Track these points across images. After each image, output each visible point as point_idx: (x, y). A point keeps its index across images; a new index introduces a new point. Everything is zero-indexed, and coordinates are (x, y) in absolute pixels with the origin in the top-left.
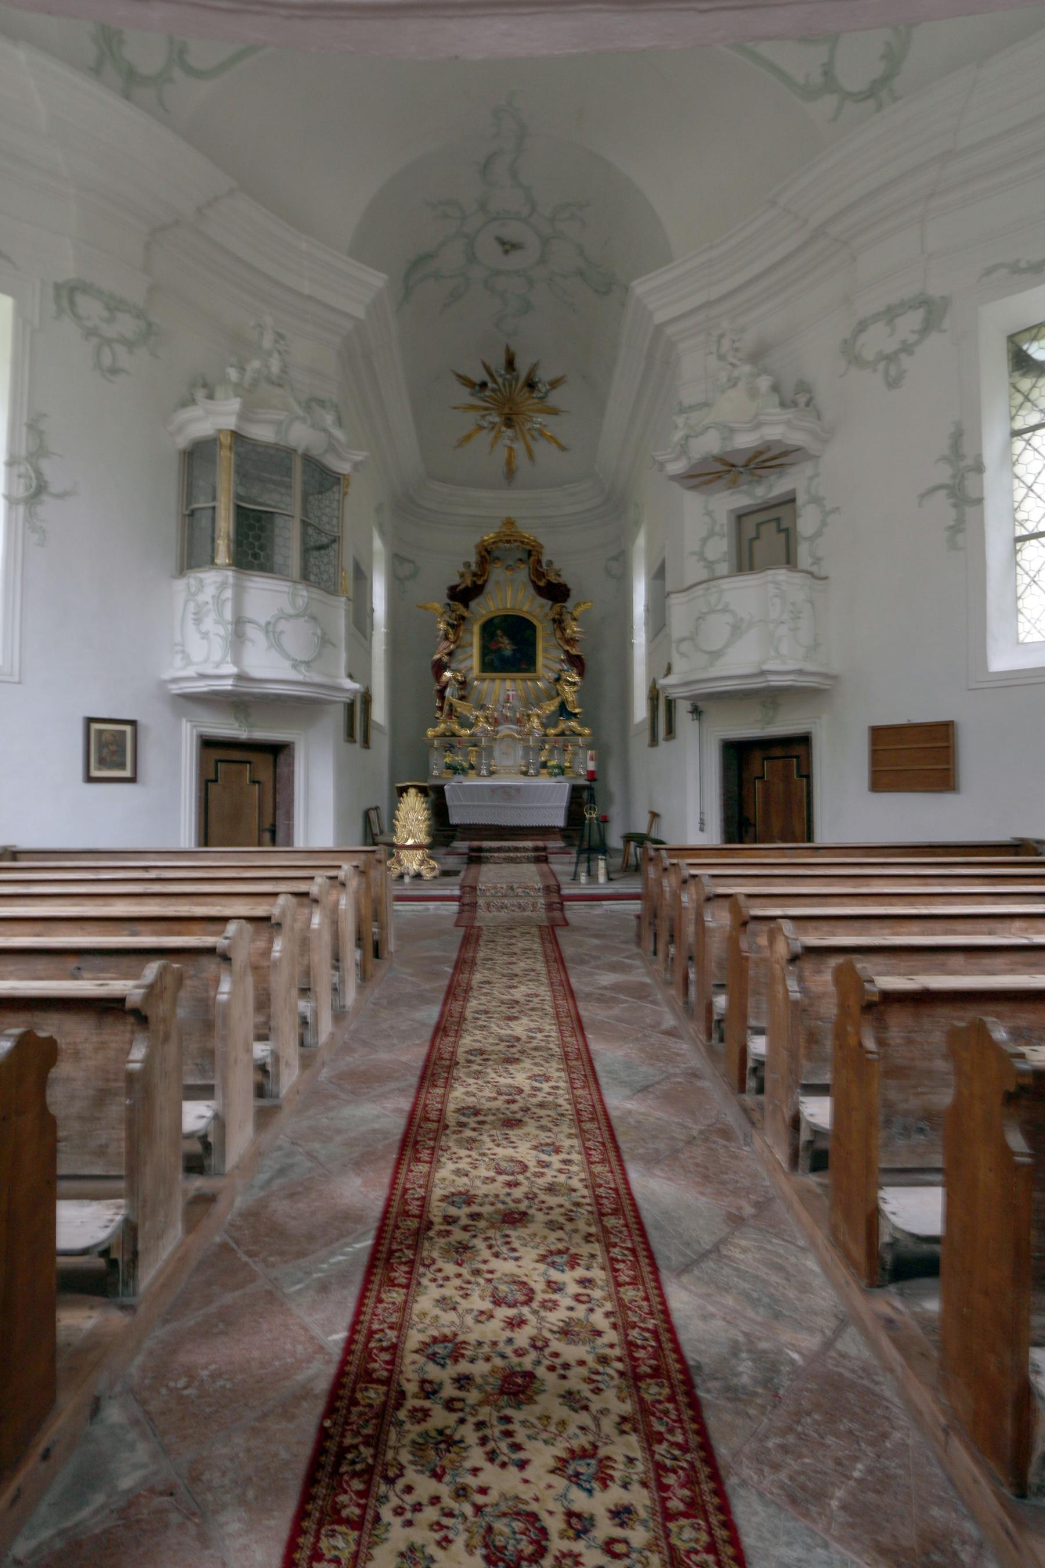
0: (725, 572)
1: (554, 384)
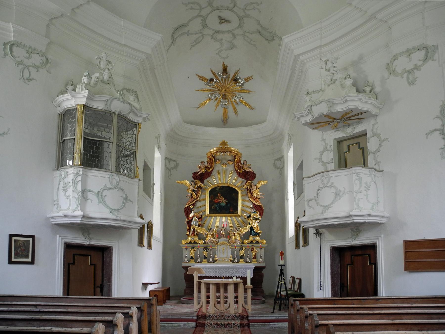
0: (333, 168)
1: (247, 80)
